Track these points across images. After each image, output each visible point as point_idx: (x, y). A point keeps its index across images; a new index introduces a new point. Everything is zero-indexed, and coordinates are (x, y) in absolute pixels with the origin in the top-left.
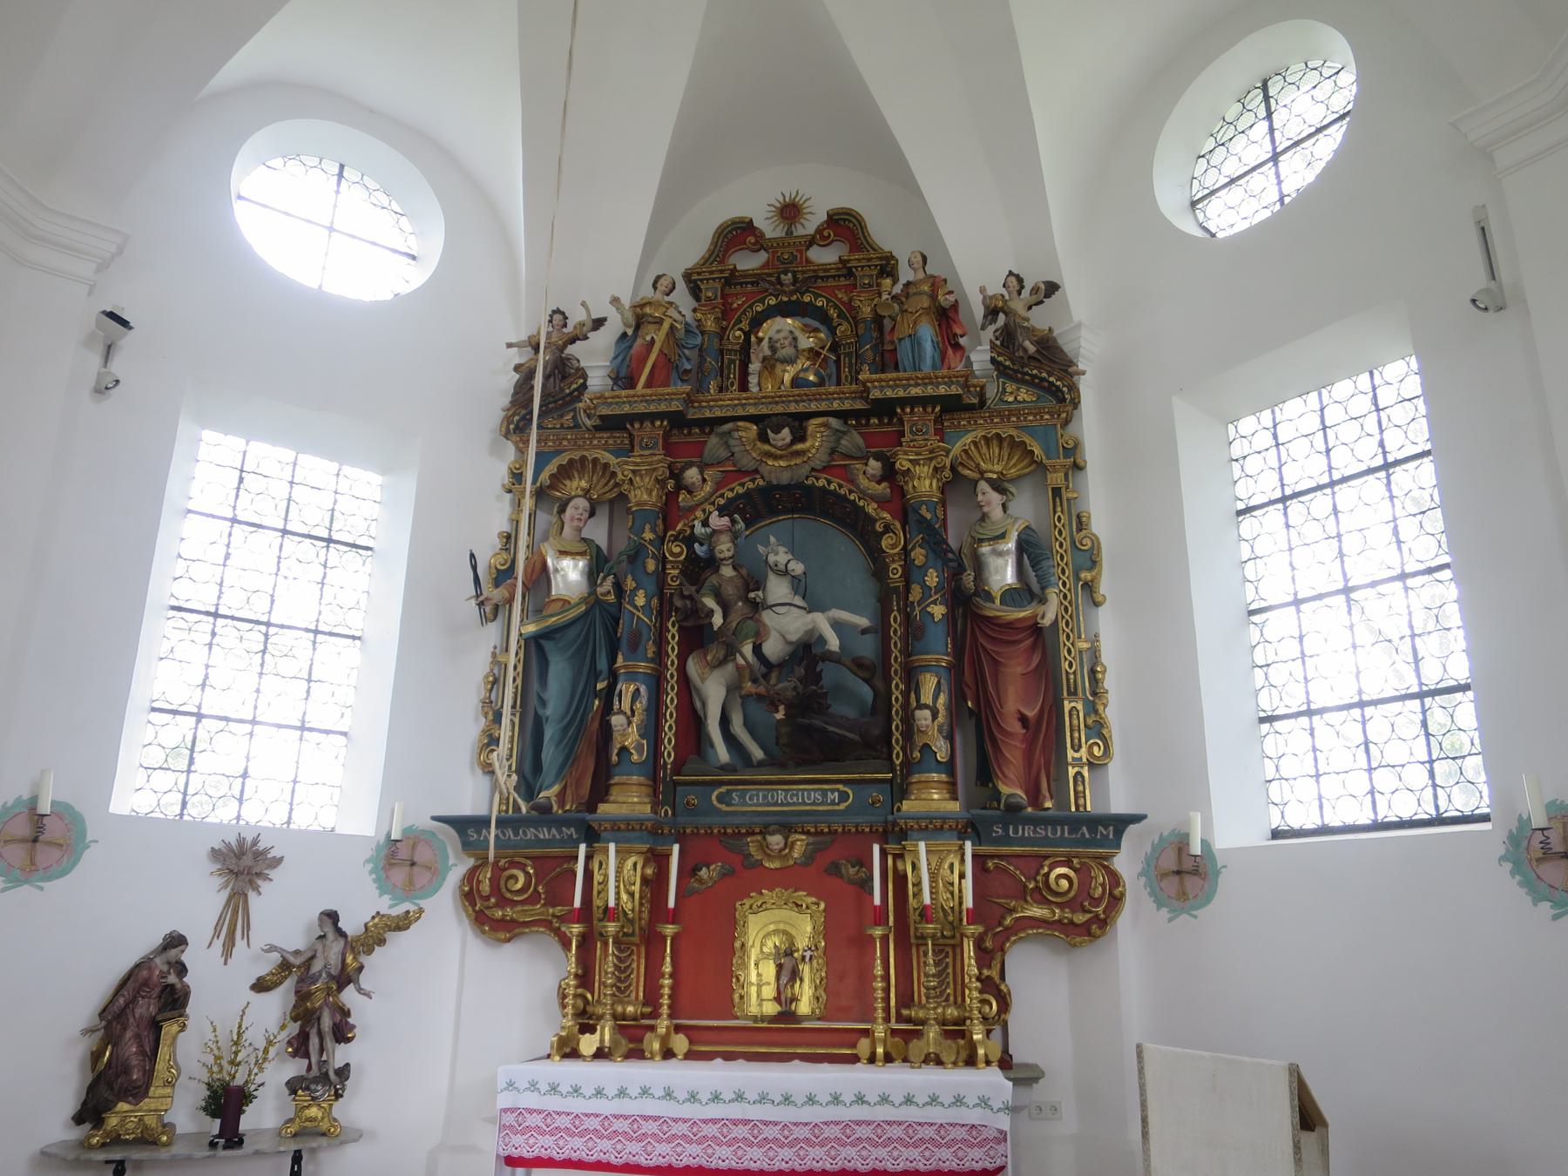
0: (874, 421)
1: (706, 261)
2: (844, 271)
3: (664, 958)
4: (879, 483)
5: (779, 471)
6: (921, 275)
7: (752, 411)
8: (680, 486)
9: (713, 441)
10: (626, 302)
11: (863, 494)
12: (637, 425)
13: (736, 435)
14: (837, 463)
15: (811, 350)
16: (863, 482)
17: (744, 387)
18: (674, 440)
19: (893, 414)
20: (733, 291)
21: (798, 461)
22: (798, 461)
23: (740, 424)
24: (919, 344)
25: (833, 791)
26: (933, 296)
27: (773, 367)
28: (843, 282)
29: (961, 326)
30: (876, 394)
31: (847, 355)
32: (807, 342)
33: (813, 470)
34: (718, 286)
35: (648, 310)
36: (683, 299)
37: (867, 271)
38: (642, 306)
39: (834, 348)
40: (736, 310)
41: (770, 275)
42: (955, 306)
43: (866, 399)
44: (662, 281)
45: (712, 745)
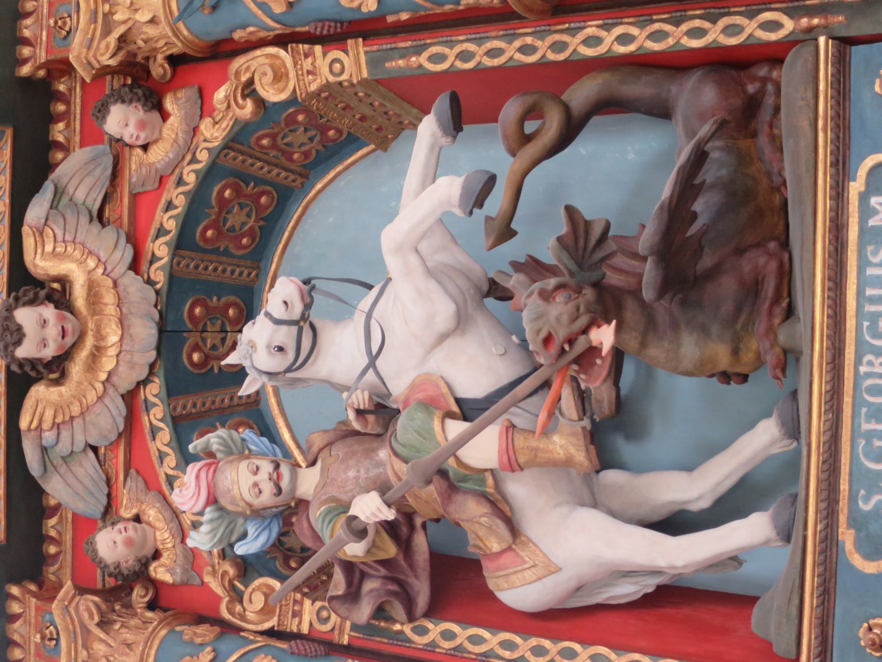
0: (58, 132)
3: (674, 167)
4: (165, 116)
5: (124, 342)
8: (140, 574)
9: (56, 489)
11: (187, 152)
14: (117, 208)
16: (159, 155)
21: (109, 298)
22: (109, 298)
23: (24, 424)
25: (866, 211)
33: (134, 267)
45: (734, 560)
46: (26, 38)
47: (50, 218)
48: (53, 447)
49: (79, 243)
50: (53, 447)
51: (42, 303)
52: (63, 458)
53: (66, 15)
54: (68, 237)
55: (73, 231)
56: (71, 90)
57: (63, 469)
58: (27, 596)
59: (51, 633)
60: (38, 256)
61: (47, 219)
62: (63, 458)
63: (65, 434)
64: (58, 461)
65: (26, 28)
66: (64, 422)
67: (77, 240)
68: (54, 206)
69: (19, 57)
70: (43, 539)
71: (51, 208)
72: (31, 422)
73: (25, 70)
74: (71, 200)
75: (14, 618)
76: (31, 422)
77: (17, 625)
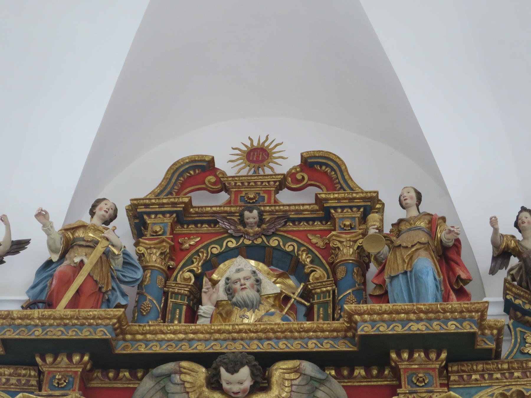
0: (360, 372)
1: (157, 194)
2: (321, 214)
6: (414, 212)
7: (201, 348)
10: (58, 222)
12: (49, 360)
13: (177, 378)
15: (277, 296)
17: (192, 316)
18: (95, 384)
19: (384, 361)
20: (185, 230)
23: (184, 364)
24: (418, 279)
26: (431, 231)
27: (229, 314)
28: (318, 226)
29: (465, 269)
30: (364, 329)
31: (320, 304)
32: (272, 287)
34: (168, 220)
35: (80, 234)
36: (122, 232)
37: (348, 213)
38: (74, 229)
39: (307, 294)
40: (188, 250)
41: (231, 213)
42: (457, 244)
43: (352, 340)
44: (102, 205)
46: (413, 355)
47: (305, 376)
48: (170, 381)
49: (291, 395)
50: (170, 381)
51: (253, 379)
52: (164, 387)
53: (426, 382)
54: (294, 388)
55: (297, 390)
56: (386, 378)
57: (158, 387)
58: (83, 366)
59: (62, 384)
60: (282, 371)
61: (305, 375)
62: (164, 387)
63: (178, 389)
64: (162, 384)
65: (419, 355)
66: (185, 388)
67: (292, 393)
68: (312, 378)
69: (402, 351)
70: (117, 369)
71: (311, 377)
72: (184, 368)
73: (394, 355)
74: (316, 388)
75: (70, 358)
76: (184, 368)
77: (65, 359)
